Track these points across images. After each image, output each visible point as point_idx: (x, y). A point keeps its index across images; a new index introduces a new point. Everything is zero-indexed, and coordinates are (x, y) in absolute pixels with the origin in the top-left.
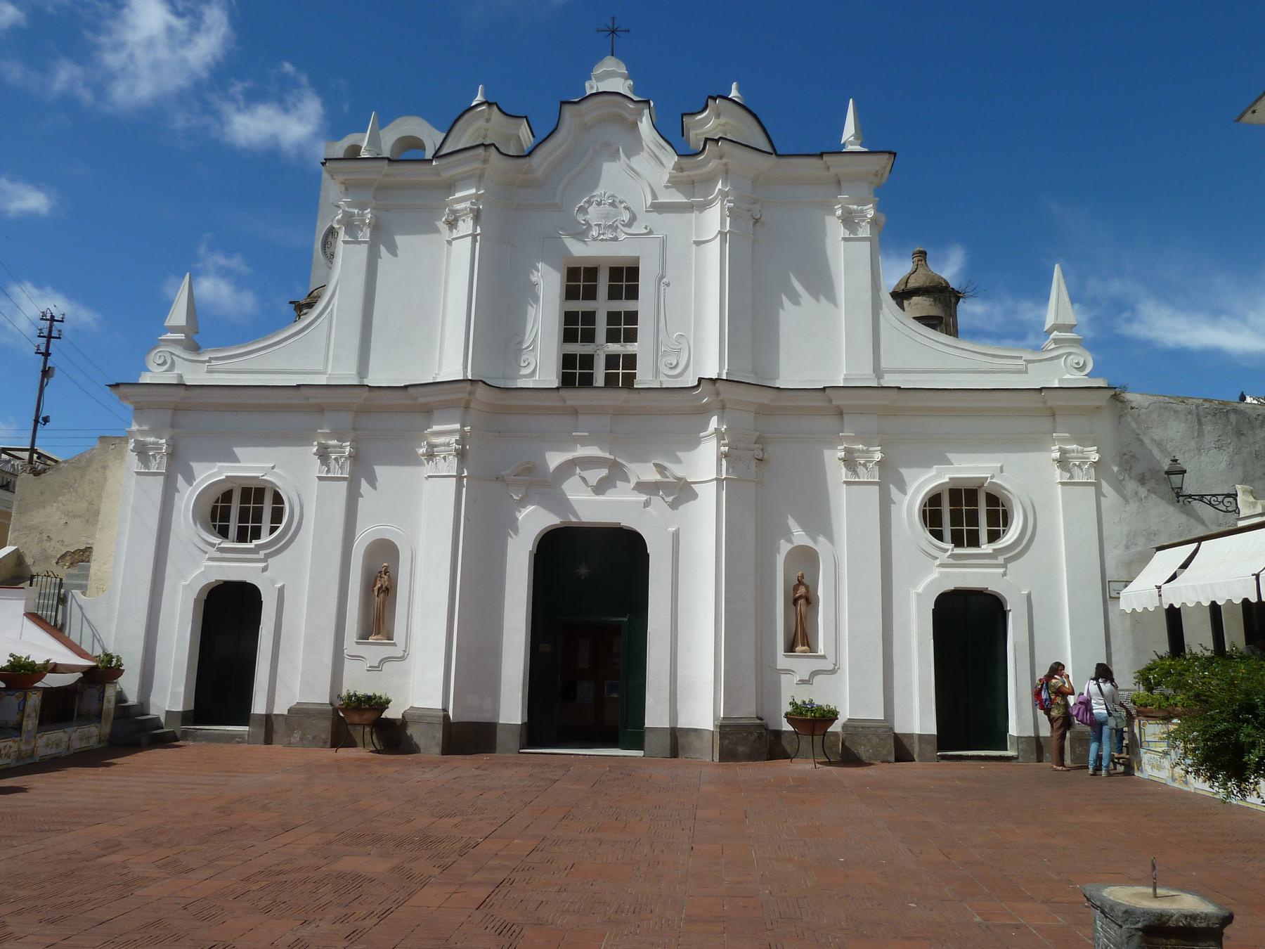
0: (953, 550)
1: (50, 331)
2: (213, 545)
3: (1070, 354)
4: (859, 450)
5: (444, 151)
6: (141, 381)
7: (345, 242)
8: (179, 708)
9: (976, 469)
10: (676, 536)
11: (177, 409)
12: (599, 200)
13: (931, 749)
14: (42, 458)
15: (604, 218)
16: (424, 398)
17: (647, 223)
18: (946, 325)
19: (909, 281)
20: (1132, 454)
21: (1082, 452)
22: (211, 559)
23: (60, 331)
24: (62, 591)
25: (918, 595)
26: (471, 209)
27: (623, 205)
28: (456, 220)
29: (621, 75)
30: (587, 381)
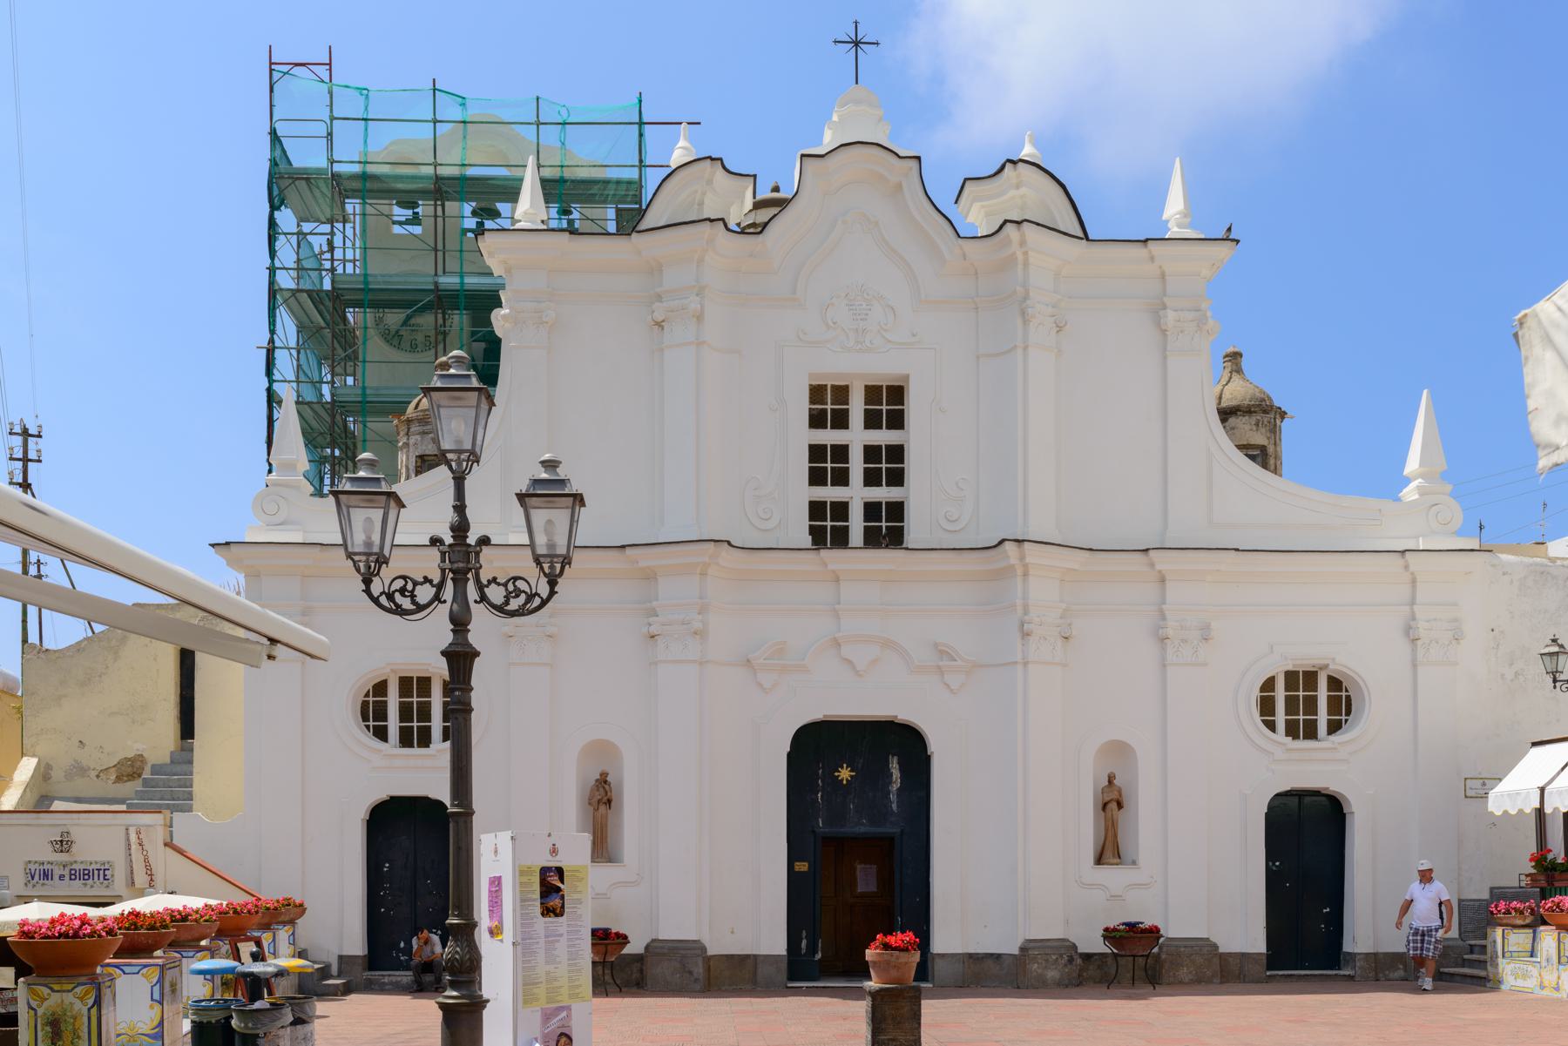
1: (25, 451)
23: (39, 451)
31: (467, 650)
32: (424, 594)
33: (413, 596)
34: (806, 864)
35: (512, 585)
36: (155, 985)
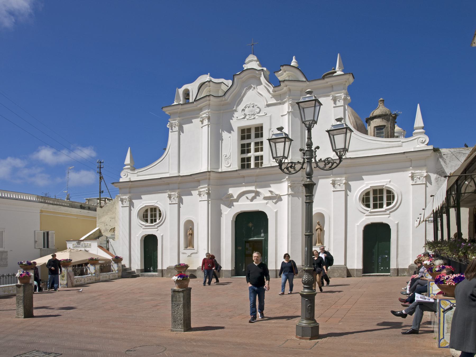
0: (370, 210)
2: (143, 225)
3: (420, 137)
4: (338, 180)
5: (197, 98)
6: (120, 181)
7: (171, 132)
8: (139, 268)
9: (380, 182)
10: (276, 213)
11: (130, 188)
12: (249, 106)
13: (360, 273)
14: (109, 200)
15: (251, 111)
16: (197, 178)
17: (265, 112)
18: (387, 128)
19: (374, 113)
20: (442, 171)
21: (421, 173)
22: (143, 229)
24: (107, 239)
25: (358, 226)
26: (206, 117)
27: (257, 106)
28: (203, 120)
29: (255, 61)
30: (249, 166)
31: (312, 183)
32: (298, 167)
33: (294, 168)
34: (241, 247)
35: (327, 161)
36: (442, 339)
